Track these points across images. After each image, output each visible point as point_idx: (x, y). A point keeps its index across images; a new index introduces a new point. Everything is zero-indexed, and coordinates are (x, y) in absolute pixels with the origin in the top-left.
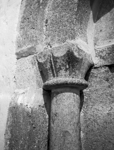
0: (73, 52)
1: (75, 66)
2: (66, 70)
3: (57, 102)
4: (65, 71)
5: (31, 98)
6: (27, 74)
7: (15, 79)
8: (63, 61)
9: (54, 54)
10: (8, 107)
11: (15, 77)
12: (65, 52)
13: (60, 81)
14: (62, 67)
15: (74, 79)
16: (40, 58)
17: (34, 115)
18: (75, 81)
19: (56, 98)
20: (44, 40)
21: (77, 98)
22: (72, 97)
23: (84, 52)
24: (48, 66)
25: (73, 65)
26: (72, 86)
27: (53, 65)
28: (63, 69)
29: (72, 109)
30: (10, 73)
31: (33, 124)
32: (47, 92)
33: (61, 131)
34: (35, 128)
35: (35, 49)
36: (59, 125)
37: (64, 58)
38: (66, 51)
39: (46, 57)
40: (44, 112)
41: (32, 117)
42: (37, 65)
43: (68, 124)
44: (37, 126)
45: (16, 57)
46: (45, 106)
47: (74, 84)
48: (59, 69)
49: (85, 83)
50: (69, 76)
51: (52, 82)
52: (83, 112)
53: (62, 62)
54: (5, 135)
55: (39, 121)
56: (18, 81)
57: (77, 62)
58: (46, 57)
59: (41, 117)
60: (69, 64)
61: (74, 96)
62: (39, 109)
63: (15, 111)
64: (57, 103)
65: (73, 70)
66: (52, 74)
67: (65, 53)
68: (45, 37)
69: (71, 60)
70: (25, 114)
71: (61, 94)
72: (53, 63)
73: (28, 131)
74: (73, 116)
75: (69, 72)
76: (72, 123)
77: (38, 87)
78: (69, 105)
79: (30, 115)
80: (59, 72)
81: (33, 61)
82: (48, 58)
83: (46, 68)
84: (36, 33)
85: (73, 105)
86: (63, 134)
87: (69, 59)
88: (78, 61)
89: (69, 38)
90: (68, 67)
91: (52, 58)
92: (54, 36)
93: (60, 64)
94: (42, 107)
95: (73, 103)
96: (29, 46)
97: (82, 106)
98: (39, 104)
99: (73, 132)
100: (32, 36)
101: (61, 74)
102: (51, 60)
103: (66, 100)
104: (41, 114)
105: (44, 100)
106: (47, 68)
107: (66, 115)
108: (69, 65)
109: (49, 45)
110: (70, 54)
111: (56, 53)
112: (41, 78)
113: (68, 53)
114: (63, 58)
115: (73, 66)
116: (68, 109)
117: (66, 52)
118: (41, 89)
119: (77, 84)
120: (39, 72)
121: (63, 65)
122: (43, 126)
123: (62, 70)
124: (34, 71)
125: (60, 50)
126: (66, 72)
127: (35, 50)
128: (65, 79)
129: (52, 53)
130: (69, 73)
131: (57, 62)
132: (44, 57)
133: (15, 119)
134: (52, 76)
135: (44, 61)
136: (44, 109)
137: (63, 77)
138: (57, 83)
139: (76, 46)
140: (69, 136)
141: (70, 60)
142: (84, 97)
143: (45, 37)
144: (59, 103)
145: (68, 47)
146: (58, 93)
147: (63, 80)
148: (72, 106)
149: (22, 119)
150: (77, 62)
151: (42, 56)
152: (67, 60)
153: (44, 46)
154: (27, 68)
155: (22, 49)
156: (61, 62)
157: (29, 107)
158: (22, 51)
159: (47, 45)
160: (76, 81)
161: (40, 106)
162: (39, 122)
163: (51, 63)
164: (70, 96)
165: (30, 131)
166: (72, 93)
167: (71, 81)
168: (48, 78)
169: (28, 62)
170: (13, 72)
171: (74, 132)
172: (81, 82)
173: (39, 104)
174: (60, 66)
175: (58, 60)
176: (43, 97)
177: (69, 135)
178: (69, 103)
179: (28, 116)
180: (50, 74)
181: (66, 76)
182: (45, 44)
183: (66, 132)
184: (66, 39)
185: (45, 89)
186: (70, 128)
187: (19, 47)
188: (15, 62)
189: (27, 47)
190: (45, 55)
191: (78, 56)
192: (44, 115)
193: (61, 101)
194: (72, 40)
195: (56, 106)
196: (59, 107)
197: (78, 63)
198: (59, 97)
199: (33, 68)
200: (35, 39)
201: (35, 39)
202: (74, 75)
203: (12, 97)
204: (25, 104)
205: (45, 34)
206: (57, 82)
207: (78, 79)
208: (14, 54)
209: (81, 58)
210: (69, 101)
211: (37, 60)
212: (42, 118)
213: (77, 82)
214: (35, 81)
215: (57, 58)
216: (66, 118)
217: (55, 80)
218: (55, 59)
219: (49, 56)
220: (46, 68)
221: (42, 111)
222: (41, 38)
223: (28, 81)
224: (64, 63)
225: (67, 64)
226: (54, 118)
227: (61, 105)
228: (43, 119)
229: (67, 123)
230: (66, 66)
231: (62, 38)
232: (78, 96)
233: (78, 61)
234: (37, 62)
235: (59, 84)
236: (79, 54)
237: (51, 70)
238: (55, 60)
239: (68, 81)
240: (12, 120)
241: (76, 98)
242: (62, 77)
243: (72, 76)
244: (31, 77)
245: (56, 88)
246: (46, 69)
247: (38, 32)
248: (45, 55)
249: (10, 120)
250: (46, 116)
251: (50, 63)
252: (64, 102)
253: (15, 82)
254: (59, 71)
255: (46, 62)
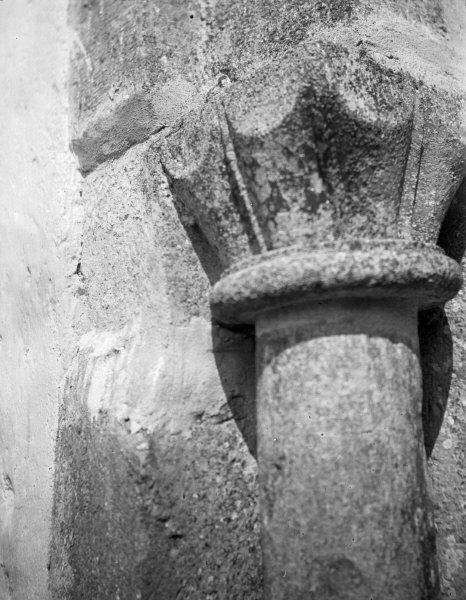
0: (334, 97)
1: (364, 177)
2: (313, 204)
3: (278, 391)
4: (305, 215)
5: (147, 369)
6: (127, 249)
7: (84, 279)
8: (289, 154)
9: (236, 125)
10: (56, 426)
11: (83, 269)
12: (288, 102)
13: (279, 278)
14: (286, 189)
15: (359, 255)
16: (174, 157)
17: (169, 469)
18: (365, 264)
19: (275, 371)
20: (200, 51)
21: (395, 362)
22: (365, 359)
23: (418, 85)
24: (217, 193)
25: (349, 173)
26: (359, 293)
27: (242, 185)
28: (295, 200)
29: (367, 429)
30: (54, 250)
31: (165, 520)
32: (237, 336)
33: (309, 561)
34: (180, 537)
35: (150, 106)
36: (297, 524)
37: (288, 136)
38: (295, 96)
39: (204, 145)
40: (231, 448)
41: (158, 481)
42: (166, 193)
43: (349, 519)
44: (191, 529)
45: (73, 160)
46: (230, 415)
47: (364, 283)
48: (272, 208)
49: (431, 271)
50: (331, 237)
51: (241, 283)
52: (454, 430)
53: (280, 165)
54: (49, 568)
55: (205, 496)
56: (93, 287)
57: (371, 148)
58: (204, 145)
59: (212, 473)
60: (326, 167)
61: (373, 352)
62: (195, 435)
63: (79, 443)
64: (279, 399)
65: (355, 199)
66: (245, 236)
67: (289, 108)
68: (203, 32)
69: (331, 145)
70: (122, 471)
71: (298, 348)
72: (238, 176)
73: (140, 558)
74: (378, 471)
75: (334, 217)
76: (368, 510)
77: (182, 317)
78: (347, 406)
79: (143, 472)
80: (276, 224)
81: (147, 175)
82: (210, 150)
83: (209, 205)
84: (151, 17)
85: (371, 407)
86: (320, 579)
87: (317, 137)
88: (377, 147)
89: (318, 14)
90: (318, 187)
91: (230, 146)
92: (247, 19)
93: (271, 179)
94: (214, 420)
95: (370, 393)
96: (124, 96)
97: (447, 395)
98: (192, 407)
99: (378, 566)
100: (130, 39)
101: (288, 234)
102: (227, 162)
103: (325, 379)
104: (213, 460)
105: (225, 383)
106: (217, 204)
107: (330, 466)
108: (323, 175)
109: (226, 71)
110: (319, 109)
111: (245, 112)
112: (194, 263)
113: (309, 107)
114: (284, 140)
115: (351, 180)
116: (343, 429)
117: (293, 102)
118: (199, 323)
119: (382, 283)
120: (184, 232)
121: (289, 179)
122: (229, 520)
123: (288, 209)
124: (154, 232)
125: (264, 93)
126: (315, 217)
127: (153, 116)
128: (309, 260)
129: (226, 116)
130: (331, 222)
131: (255, 164)
132: (194, 148)
133: (85, 491)
134: (247, 247)
135: (193, 167)
136: (229, 428)
137: (304, 250)
138: (262, 288)
139: (354, 55)
140: (357, 586)
141: (325, 147)
142: (451, 342)
143: (203, 32)
144: (289, 399)
145: (302, 71)
146: (281, 343)
147: (295, 268)
148: (366, 411)
149: (110, 492)
150: (371, 148)
151: (183, 145)
152: (304, 146)
153: (203, 87)
154: (126, 217)
155: (95, 119)
156: (274, 164)
157: (135, 427)
158: (97, 127)
159: (218, 77)
160: (372, 267)
161: (199, 416)
162: (201, 503)
163: (230, 174)
164: (347, 355)
165: (151, 557)
166: (363, 338)
167: (343, 269)
168: (228, 259)
169: (125, 184)
170: (65, 244)
171: (384, 564)
172: (406, 267)
173: (196, 408)
174: (273, 185)
175: (259, 155)
176: (219, 365)
177: (357, 581)
178: (348, 396)
179: (135, 478)
180: (235, 237)
181: (316, 242)
182: (210, 72)
183: (342, 563)
184: (305, 24)
185: (227, 322)
186: (359, 539)
187: (85, 106)
188: (74, 188)
189: (113, 106)
190: (196, 137)
191: (371, 117)
192: (234, 461)
193: (302, 385)
194: (339, 24)
195: (277, 417)
196: (290, 425)
197: (378, 157)
198: (290, 366)
199: (149, 211)
200: (142, 52)
201: (144, 55)
202: (362, 229)
203: (68, 374)
204: (120, 415)
205: (204, 15)
206: (262, 282)
207: (387, 255)
208: (67, 148)
209: (393, 122)
210: (344, 387)
211: (165, 171)
212: (219, 479)
213: (377, 271)
214: (163, 286)
215: (255, 142)
216: (335, 484)
217: (254, 274)
218: (245, 145)
219: (213, 138)
220: (209, 205)
221: (214, 443)
222: (184, 42)
223: (134, 289)
224: (292, 166)
225: (311, 170)
226: (272, 486)
227: (302, 408)
228: (230, 486)
229: (343, 512)
230: (308, 184)
231: (283, 25)
232: (399, 348)
233: (377, 147)
234: (165, 178)
235: (276, 291)
236: (383, 101)
237: (237, 217)
238: (243, 155)
239: (324, 269)
240: (73, 498)
241: (386, 363)
242: (289, 249)
243: (349, 237)
244: (144, 264)
245: (273, 315)
246: (211, 210)
247: (158, 11)
248: (196, 137)
249: (66, 495)
250: (243, 464)
251: (223, 174)
252: (317, 394)
253: (81, 292)
254: (273, 219)
255: (204, 172)
